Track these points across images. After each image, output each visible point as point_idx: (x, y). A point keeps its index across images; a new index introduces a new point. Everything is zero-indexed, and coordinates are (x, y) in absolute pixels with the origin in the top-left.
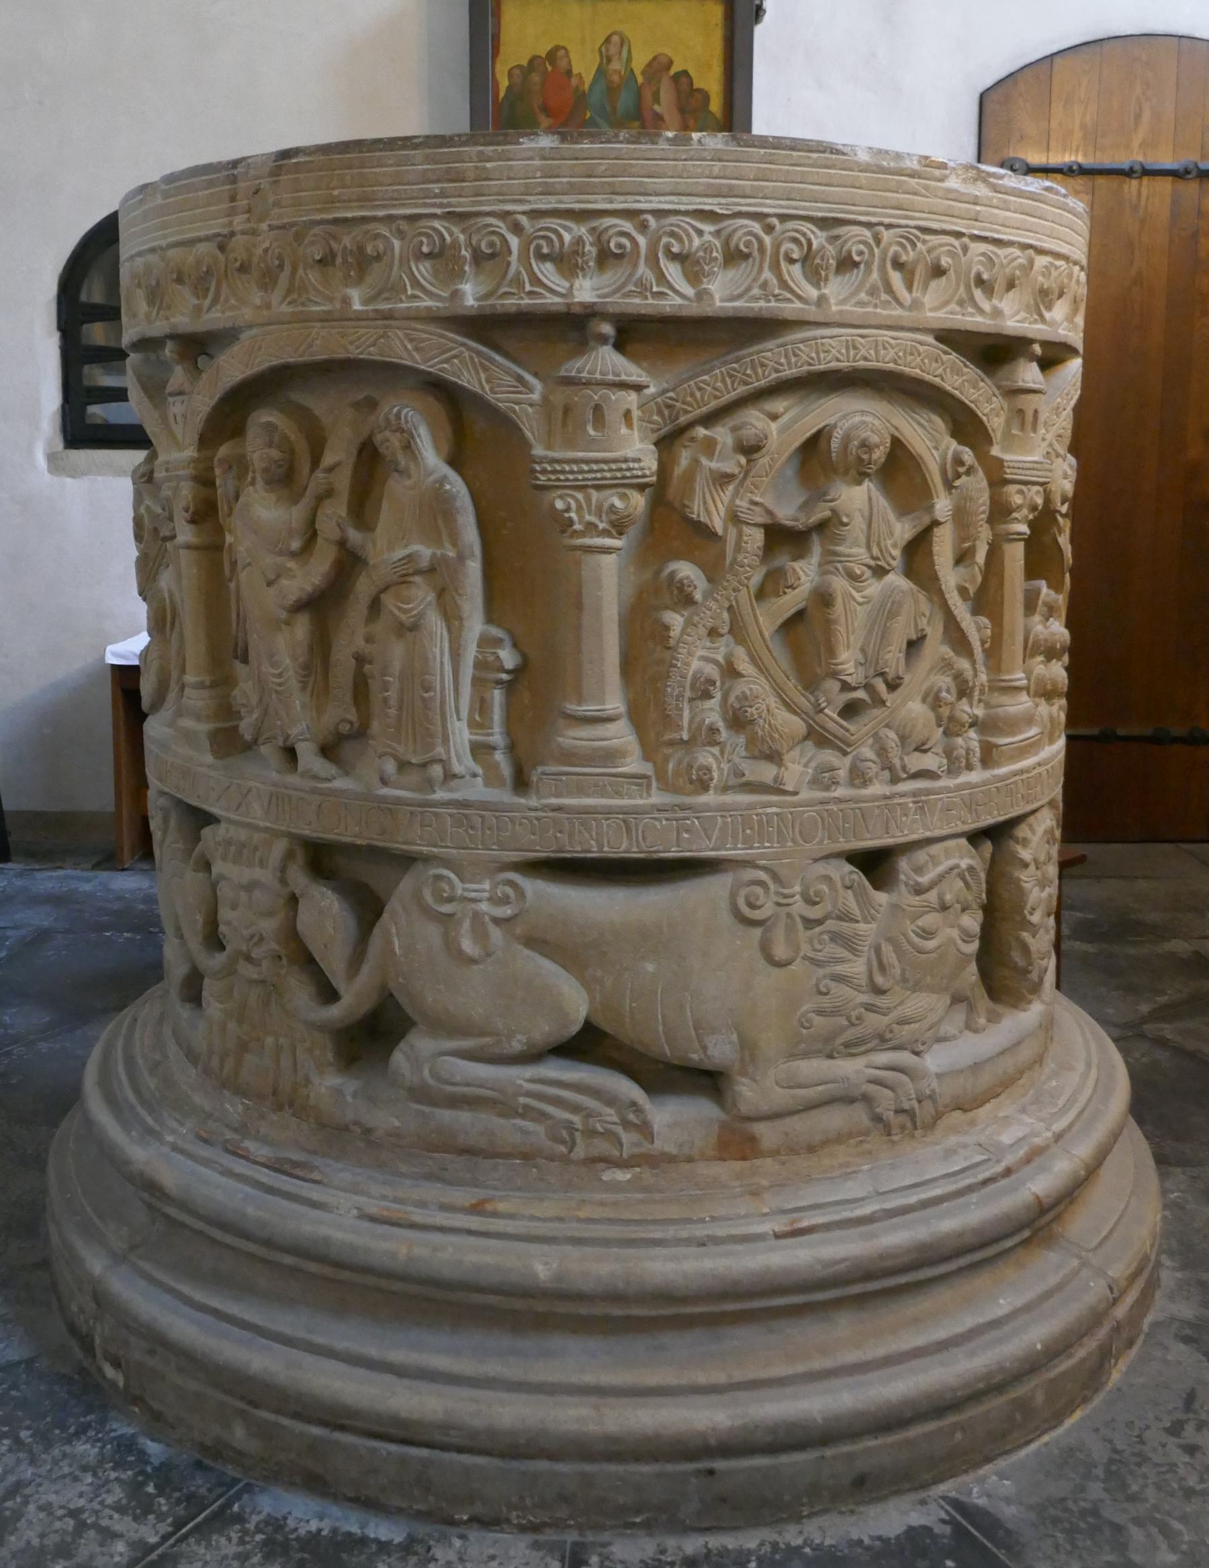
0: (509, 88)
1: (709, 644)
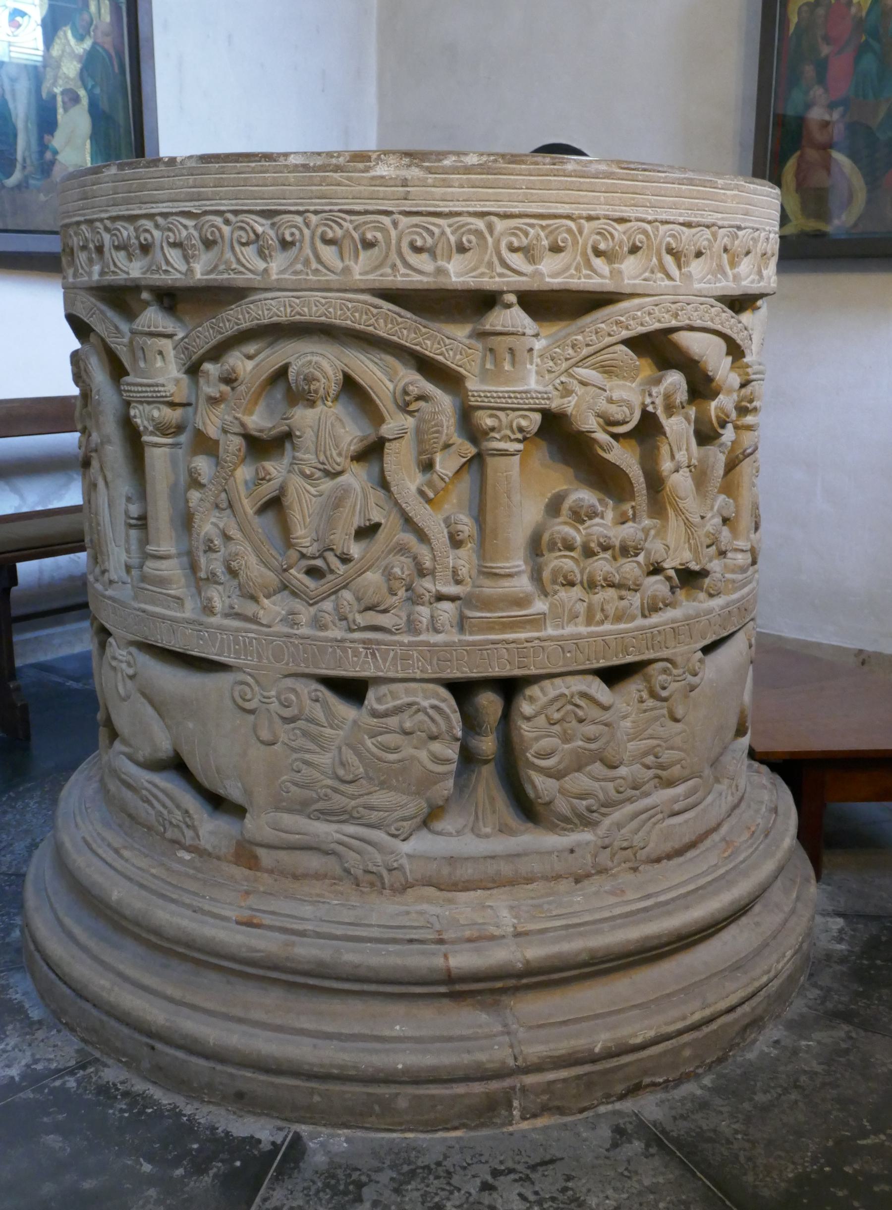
1: (217, 514)
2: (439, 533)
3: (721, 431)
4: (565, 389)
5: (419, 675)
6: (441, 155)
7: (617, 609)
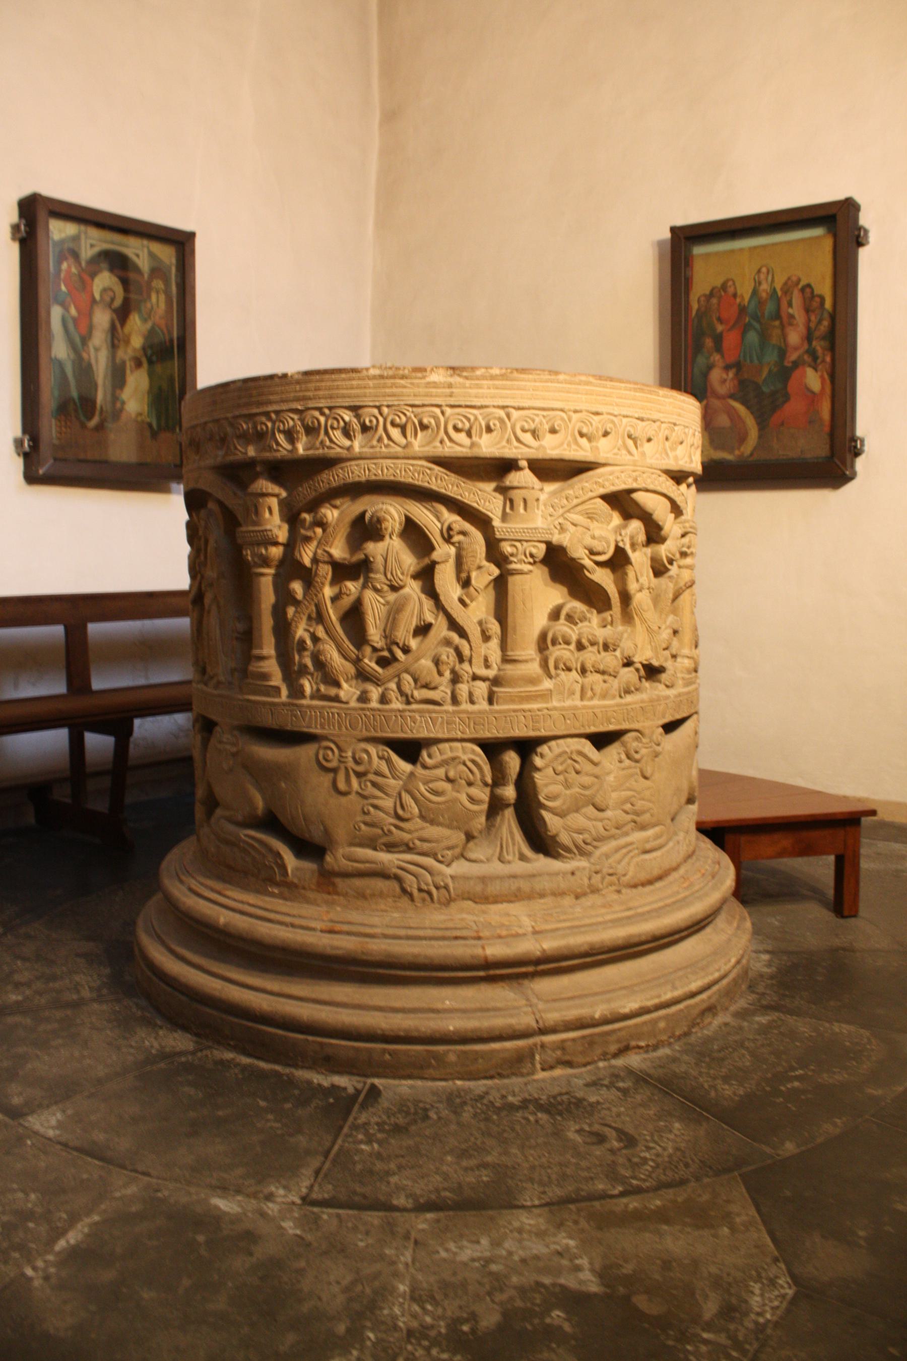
0: (698, 310)
2: (474, 632)
3: (669, 566)
4: (562, 528)
5: (459, 735)
6: (473, 369)
7: (602, 689)
